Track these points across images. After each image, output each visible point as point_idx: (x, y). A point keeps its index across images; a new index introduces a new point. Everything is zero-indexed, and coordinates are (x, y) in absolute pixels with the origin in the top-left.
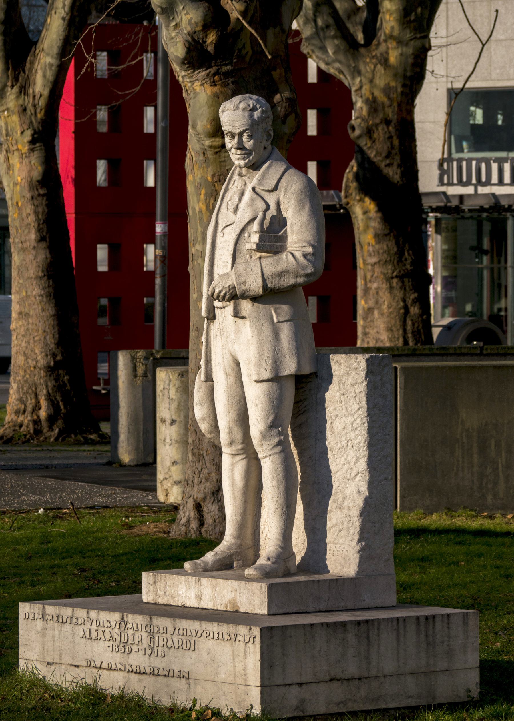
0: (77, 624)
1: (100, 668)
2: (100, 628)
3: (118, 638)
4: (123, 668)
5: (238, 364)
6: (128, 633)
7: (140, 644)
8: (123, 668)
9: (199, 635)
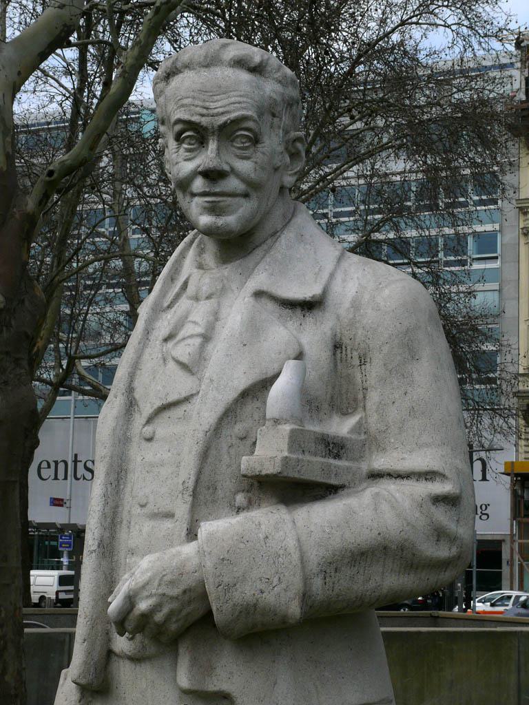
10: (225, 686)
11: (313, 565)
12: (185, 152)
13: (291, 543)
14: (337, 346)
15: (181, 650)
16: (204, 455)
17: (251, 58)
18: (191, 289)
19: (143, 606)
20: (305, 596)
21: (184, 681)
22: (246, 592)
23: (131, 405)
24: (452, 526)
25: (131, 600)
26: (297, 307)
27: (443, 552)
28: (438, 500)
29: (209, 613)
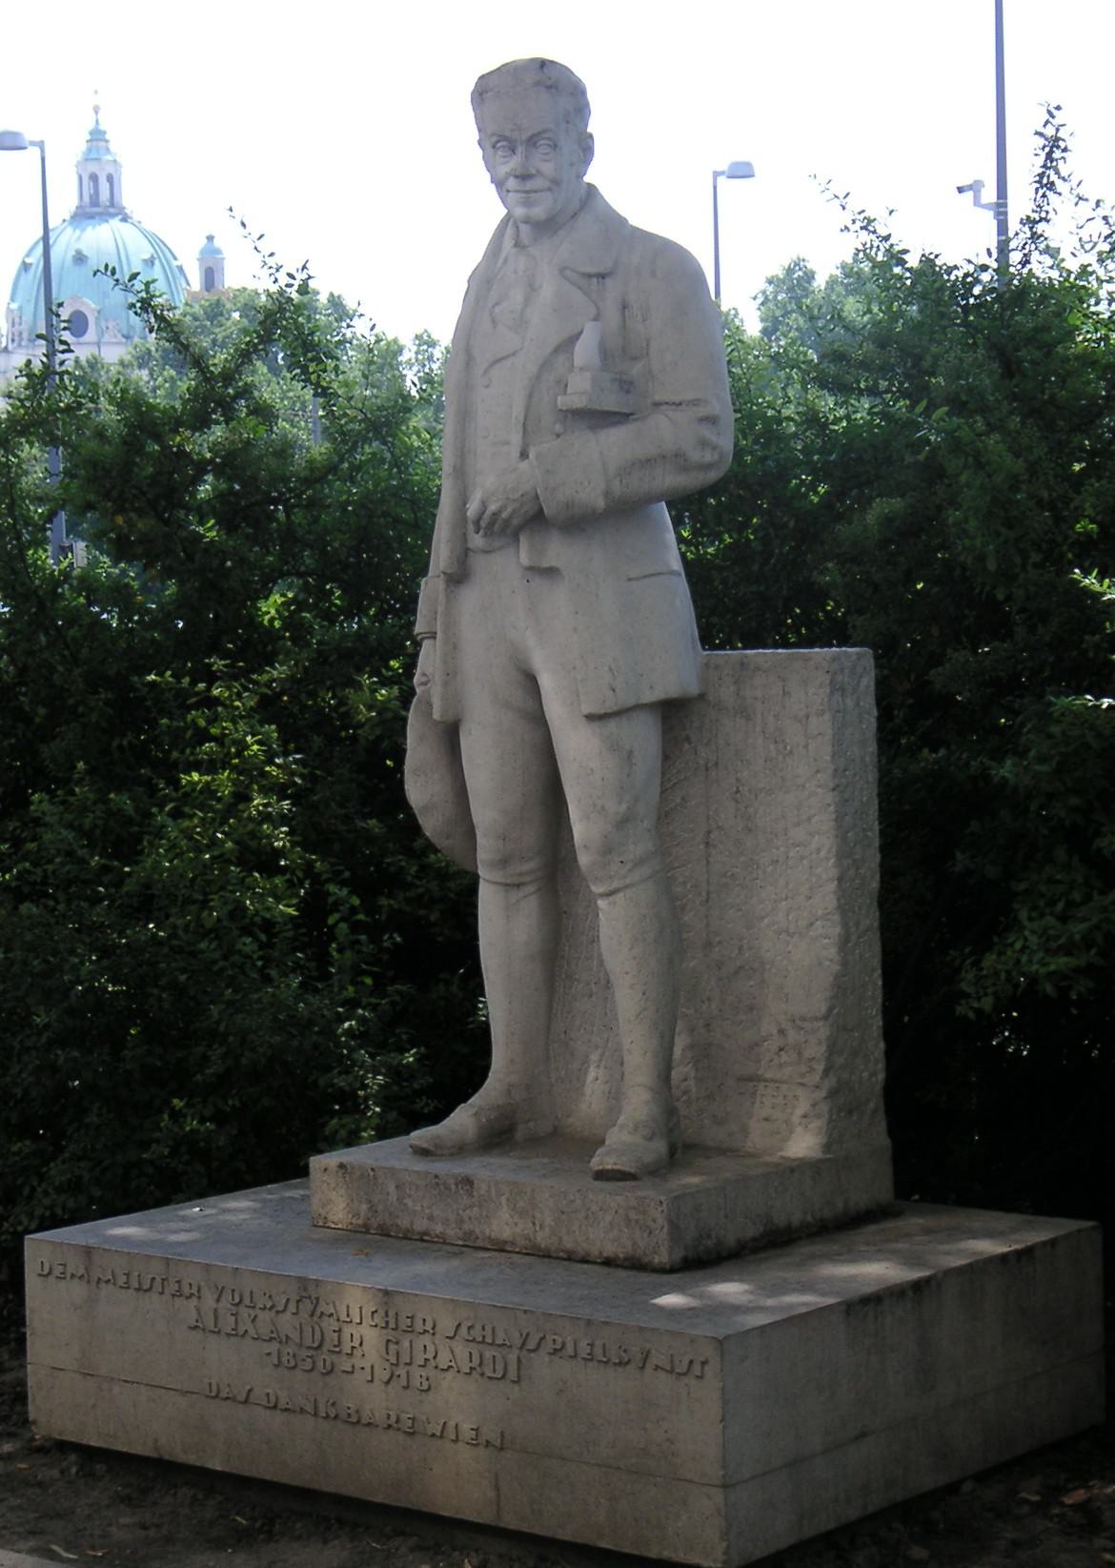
0: (178, 1294)
1: (246, 1401)
2: (242, 1309)
3: (295, 1336)
4: (309, 1408)
5: (531, 681)
6: (324, 1325)
7: (358, 1353)
8: (309, 1408)
9: (531, 1345)
10: (554, 564)
15: (522, 538)
16: (530, 396)
17: (636, 1128)
19: (492, 508)
20: (607, 494)
21: (524, 558)
24: (714, 439)
25: (484, 505)
26: (601, 504)
27: (709, 457)
29: (541, 510)
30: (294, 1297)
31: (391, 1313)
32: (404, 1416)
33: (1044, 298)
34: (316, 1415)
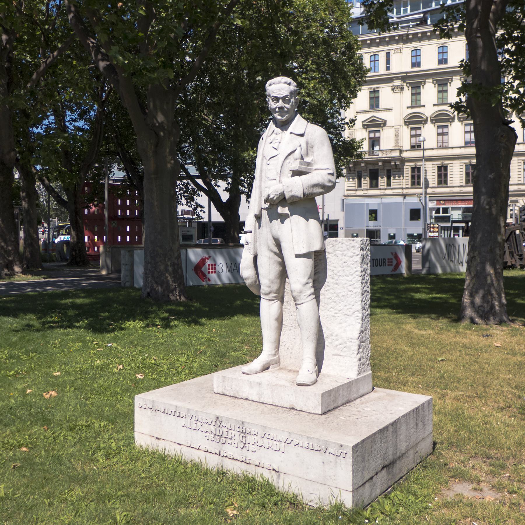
9: (288, 441)
11: (305, 188)
12: (336, 236)
13: (301, 183)
14: (307, 144)
18: (275, 132)
19: (271, 197)
20: (304, 194)
22: (293, 193)
23: (264, 156)
28: (329, 174)
29: (285, 198)
30: (214, 420)
31: (244, 428)
32: (247, 459)
33: (348, 86)
34: (220, 455)
